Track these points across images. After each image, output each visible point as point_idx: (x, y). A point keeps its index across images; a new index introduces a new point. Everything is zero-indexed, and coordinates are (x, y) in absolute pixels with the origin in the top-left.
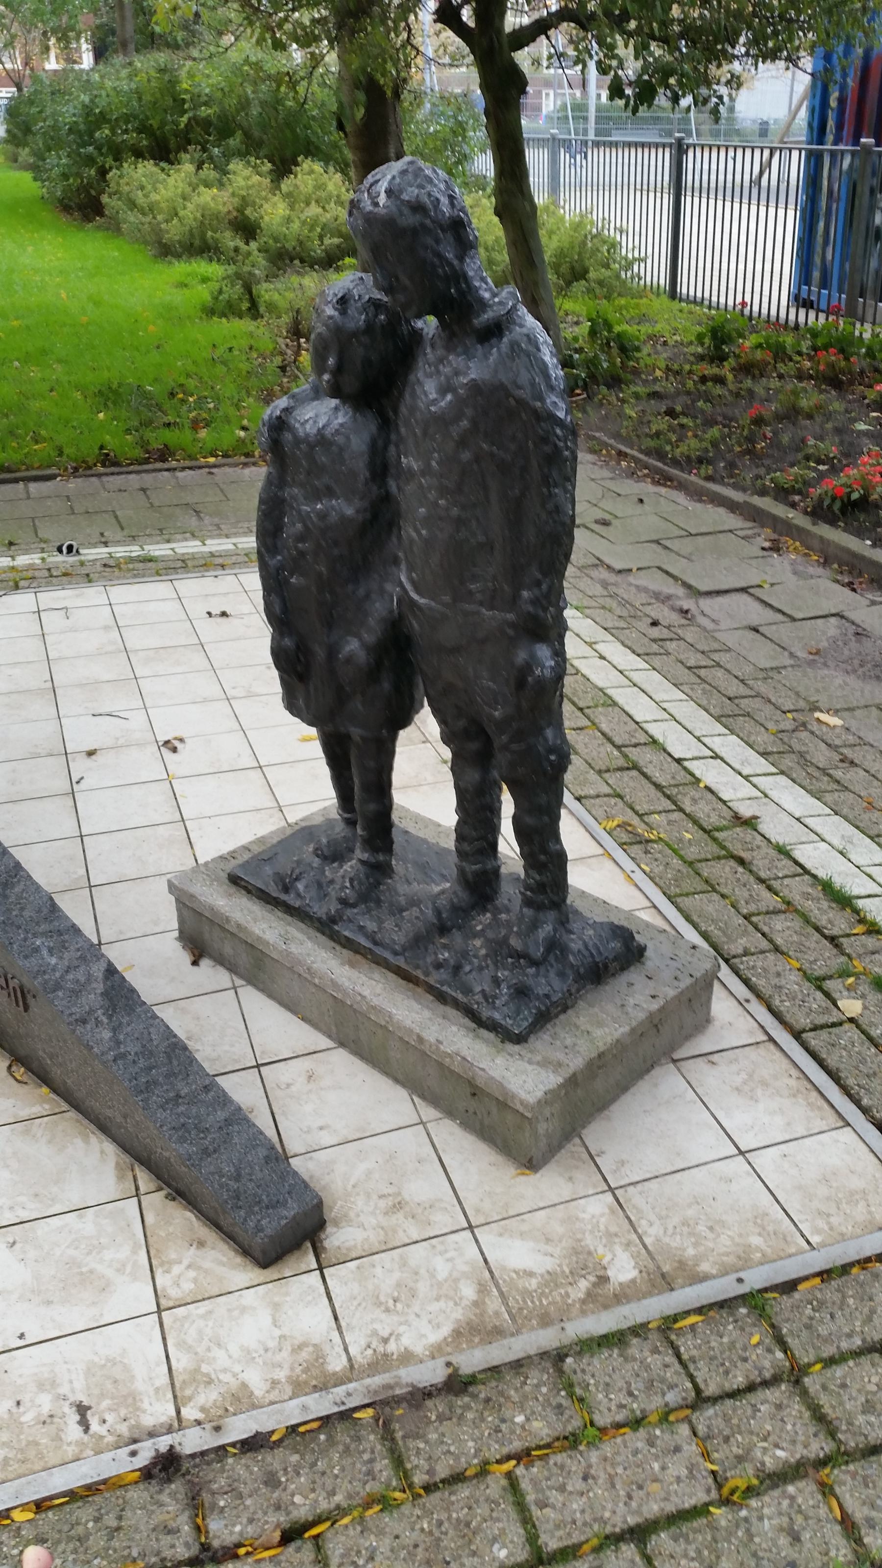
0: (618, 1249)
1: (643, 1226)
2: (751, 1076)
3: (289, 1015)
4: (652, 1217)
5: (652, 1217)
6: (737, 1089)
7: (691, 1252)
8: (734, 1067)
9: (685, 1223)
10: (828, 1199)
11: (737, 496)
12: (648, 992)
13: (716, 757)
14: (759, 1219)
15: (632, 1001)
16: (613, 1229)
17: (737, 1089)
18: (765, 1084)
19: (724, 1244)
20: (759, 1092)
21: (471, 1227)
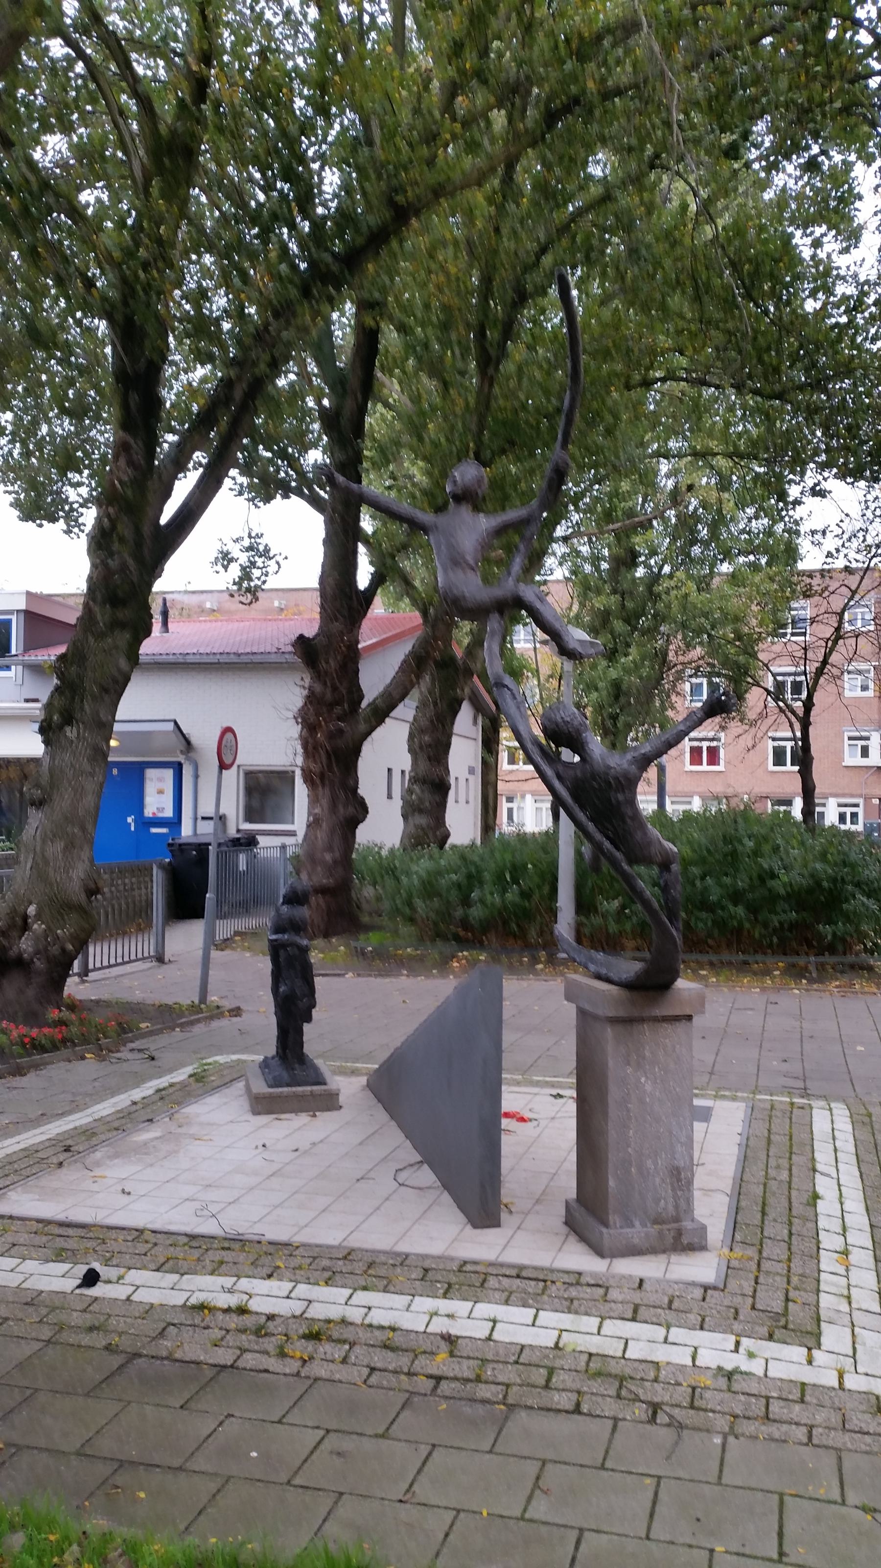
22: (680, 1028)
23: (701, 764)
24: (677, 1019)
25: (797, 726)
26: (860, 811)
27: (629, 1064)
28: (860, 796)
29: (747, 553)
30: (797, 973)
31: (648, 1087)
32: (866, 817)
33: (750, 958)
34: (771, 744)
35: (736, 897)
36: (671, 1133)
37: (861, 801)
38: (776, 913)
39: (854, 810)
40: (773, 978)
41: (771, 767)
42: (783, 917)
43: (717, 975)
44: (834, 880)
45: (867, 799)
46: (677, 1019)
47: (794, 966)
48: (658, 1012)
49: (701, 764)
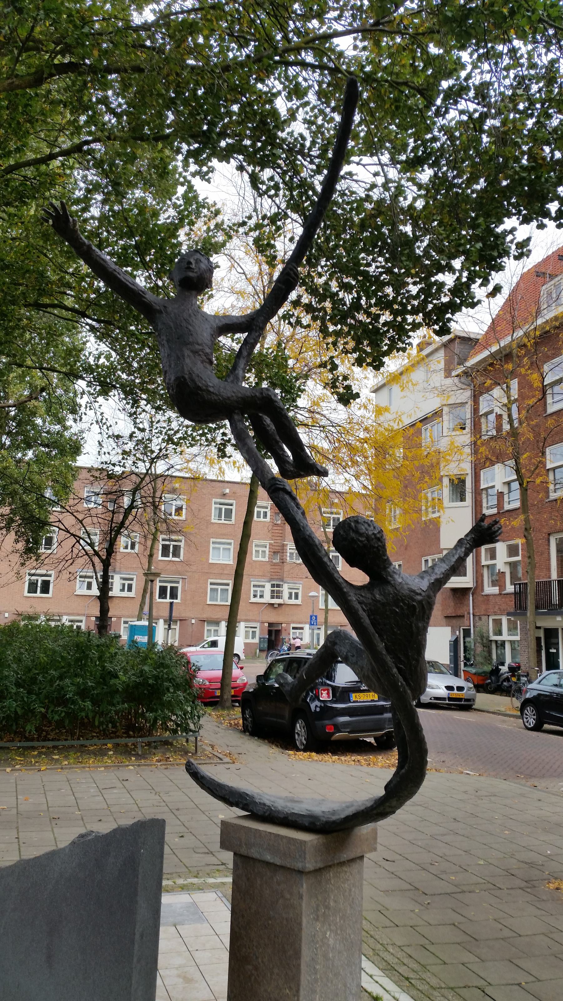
22: (355, 867)
23: (36, 592)
24: (353, 860)
25: (99, 566)
26: (257, 630)
27: (317, 919)
28: (84, 615)
29: (47, 446)
30: (127, 752)
31: (331, 942)
32: (260, 634)
33: (87, 743)
34: (28, 577)
35: (83, 693)
36: (345, 985)
37: (84, 618)
38: (114, 705)
39: (79, 624)
40: (110, 757)
41: (26, 594)
42: (119, 707)
43: (66, 757)
44: (156, 678)
45: (88, 617)
46: (353, 860)
47: (118, 745)
48: (345, 856)
49: (36, 592)
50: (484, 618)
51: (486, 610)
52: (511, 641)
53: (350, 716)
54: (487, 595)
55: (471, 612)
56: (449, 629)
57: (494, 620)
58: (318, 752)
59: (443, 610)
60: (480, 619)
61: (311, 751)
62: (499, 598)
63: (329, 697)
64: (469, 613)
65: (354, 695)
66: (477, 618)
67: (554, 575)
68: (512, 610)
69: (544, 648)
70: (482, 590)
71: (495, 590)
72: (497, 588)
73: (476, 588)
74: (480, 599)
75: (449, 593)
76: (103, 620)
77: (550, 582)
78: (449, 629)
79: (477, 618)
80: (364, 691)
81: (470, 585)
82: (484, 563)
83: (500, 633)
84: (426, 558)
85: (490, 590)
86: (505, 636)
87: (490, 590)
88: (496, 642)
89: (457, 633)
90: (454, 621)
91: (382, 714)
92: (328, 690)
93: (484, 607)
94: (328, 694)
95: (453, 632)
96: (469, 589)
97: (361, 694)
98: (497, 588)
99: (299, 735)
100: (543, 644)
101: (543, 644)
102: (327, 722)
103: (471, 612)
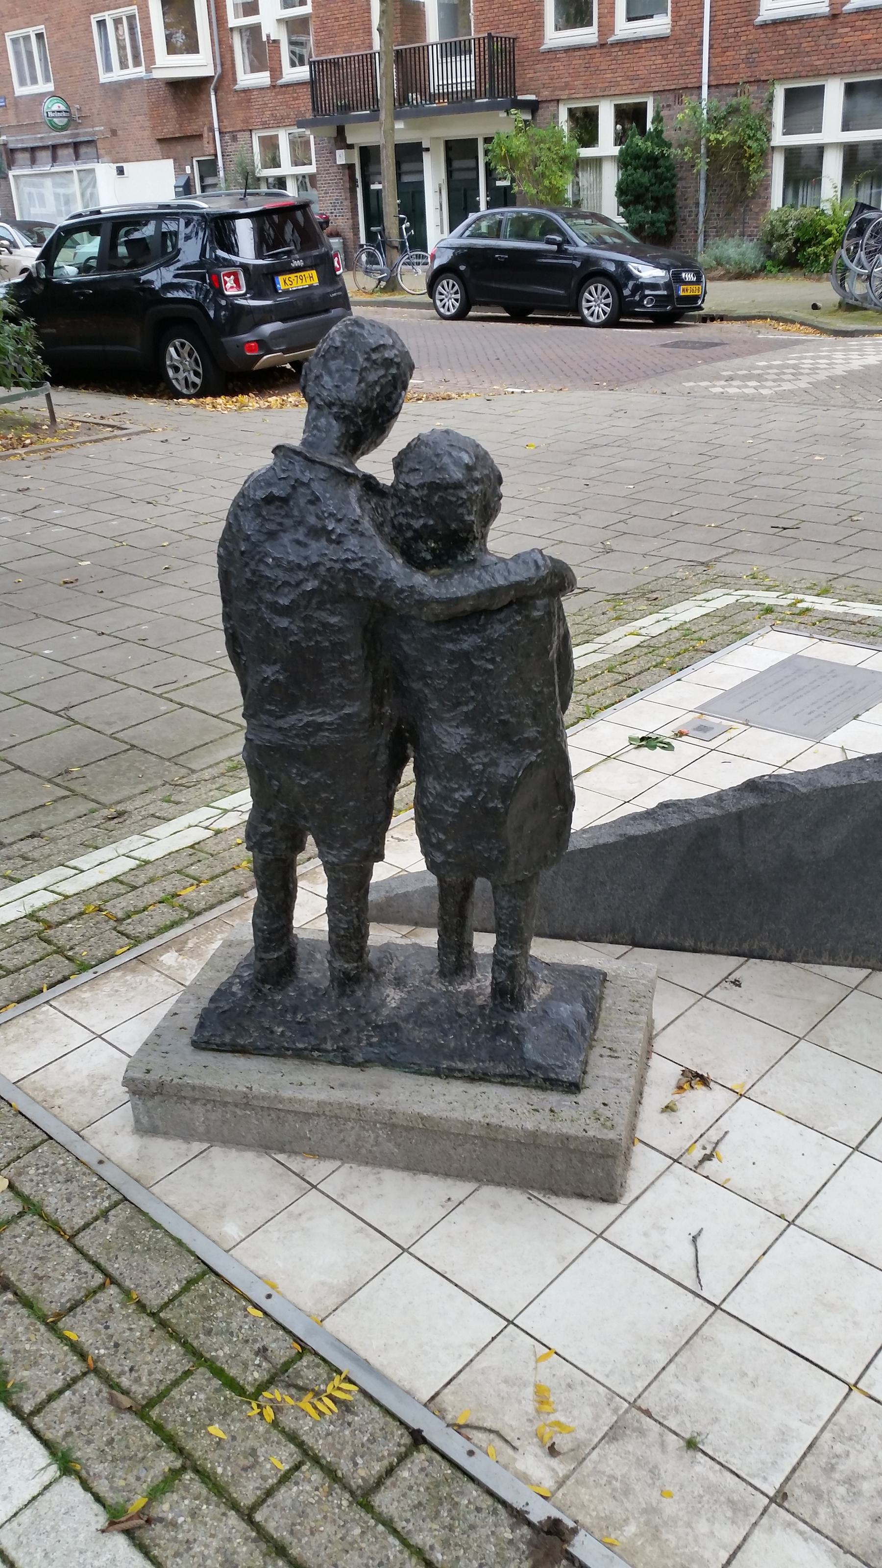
0: (174, 964)
1: (162, 979)
2: (95, 1094)
3: (572, 943)
4: (157, 984)
5: (157, 984)
6: (105, 1079)
7: (128, 978)
8: (110, 1095)
9: (134, 989)
10: (34, 1032)
11: (581, 95)
12: (181, 1016)
13: (7, 694)
14: (84, 1005)
15: (192, 1004)
16: (181, 971)
17: (105, 1079)
18: (82, 1092)
19: (107, 987)
20: (86, 1083)
21: (510, 1322)
50: (242, 137)
51: (246, 121)
52: (296, 177)
53: (283, 320)
54: (246, 91)
55: (216, 125)
56: (170, 162)
57: (262, 140)
58: (231, 393)
59: (154, 128)
60: (234, 139)
61: (215, 395)
62: (271, 94)
63: (238, 286)
64: (211, 129)
65: (281, 279)
66: (227, 137)
67: (377, 46)
68: (309, 116)
69: (360, 183)
70: (235, 81)
71: (263, 78)
72: (267, 74)
73: (221, 77)
74: (234, 99)
75: (164, 92)
76: (129, 1056)
77: (372, 56)
78: (170, 162)
79: (227, 137)
80: (298, 270)
81: (209, 72)
82: (233, 21)
83: (275, 163)
84: (99, 16)
85: (248, 78)
86: (286, 168)
87: (248, 78)
88: (267, 179)
89: (188, 169)
90: (179, 148)
91: (327, 311)
92: (235, 274)
93: (240, 115)
94: (237, 281)
95: (179, 169)
96: (206, 80)
97: (292, 276)
98: (267, 74)
99: (176, 369)
100: (358, 176)
101: (358, 176)
102: (246, 337)
103: (216, 125)
